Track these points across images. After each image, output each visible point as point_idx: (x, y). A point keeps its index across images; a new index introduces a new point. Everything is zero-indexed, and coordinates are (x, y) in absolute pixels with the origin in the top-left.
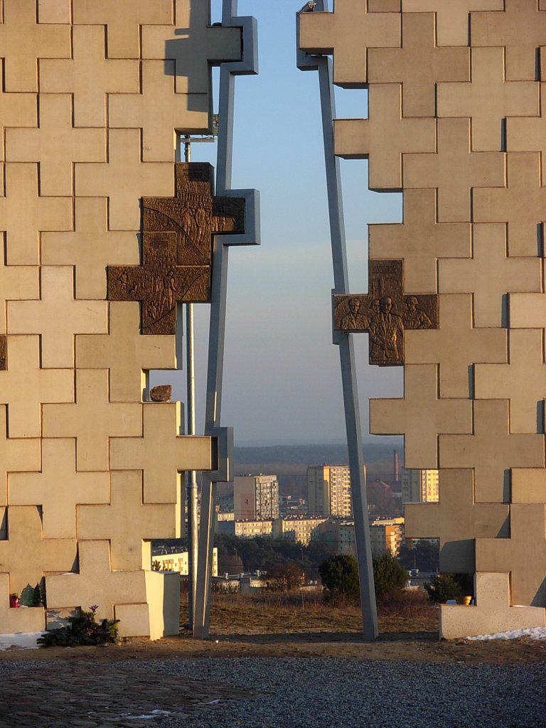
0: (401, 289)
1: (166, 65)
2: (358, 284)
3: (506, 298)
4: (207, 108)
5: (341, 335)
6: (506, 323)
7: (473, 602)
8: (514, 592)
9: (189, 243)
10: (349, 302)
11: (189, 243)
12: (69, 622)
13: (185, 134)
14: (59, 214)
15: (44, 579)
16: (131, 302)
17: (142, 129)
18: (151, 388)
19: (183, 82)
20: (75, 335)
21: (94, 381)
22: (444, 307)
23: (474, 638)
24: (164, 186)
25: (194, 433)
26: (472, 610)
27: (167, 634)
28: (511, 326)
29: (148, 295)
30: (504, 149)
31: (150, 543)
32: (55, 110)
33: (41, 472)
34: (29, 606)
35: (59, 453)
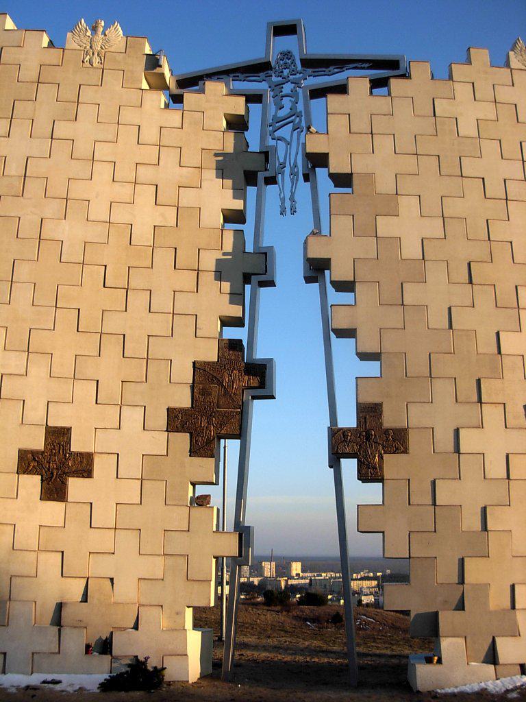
0: (381, 424)
1: (215, 275)
2: (348, 419)
3: (457, 432)
4: (242, 303)
5: (334, 463)
6: (457, 449)
7: (440, 661)
8: (469, 653)
9: (226, 393)
10: (344, 432)
11: (226, 393)
12: (128, 667)
13: (226, 322)
14: (135, 370)
15: (112, 633)
16: (184, 434)
17: (196, 315)
18: (196, 496)
19: (226, 286)
20: (143, 455)
21: (155, 489)
22: (413, 438)
23: (443, 691)
24: (210, 354)
25: (225, 531)
26: (438, 667)
27: (203, 676)
28: (461, 452)
29: (196, 430)
30: (451, 327)
31: (192, 609)
32: (138, 301)
33: (114, 553)
34: (100, 653)
35: (127, 541)
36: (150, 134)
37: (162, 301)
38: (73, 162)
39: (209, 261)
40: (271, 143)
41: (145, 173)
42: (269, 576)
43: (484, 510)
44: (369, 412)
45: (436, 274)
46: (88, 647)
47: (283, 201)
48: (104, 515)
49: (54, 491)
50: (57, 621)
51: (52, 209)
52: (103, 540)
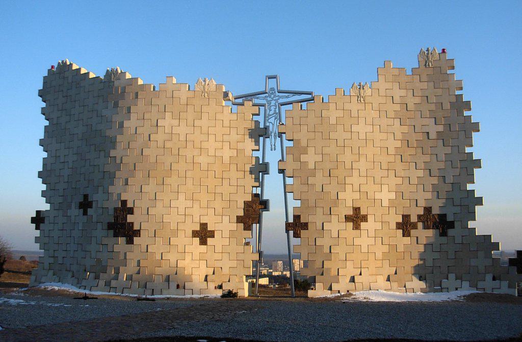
2: (291, 220)
5: (287, 231)
7: (315, 289)
19: (253, 176)
21: (234, 241)
22: (310, 226)
24: (249, 199)
27: (249, 296)
32: (226, 182)
35: (226, 256)
36: (226, 123)
37: (234, 182)
38: (202, 135)
39: (248, 168)
40: (268, 124)
41: (226, 138)
42: (298, 270)
43: (330, 246)
44: (297, 217)
45: (319, 174)
46: (215, 287)
47: (271, 146)
48: (219, 249)
49: (203, 242)
50: (206, 280)
51: (196, 152)
52: (219, 256)
